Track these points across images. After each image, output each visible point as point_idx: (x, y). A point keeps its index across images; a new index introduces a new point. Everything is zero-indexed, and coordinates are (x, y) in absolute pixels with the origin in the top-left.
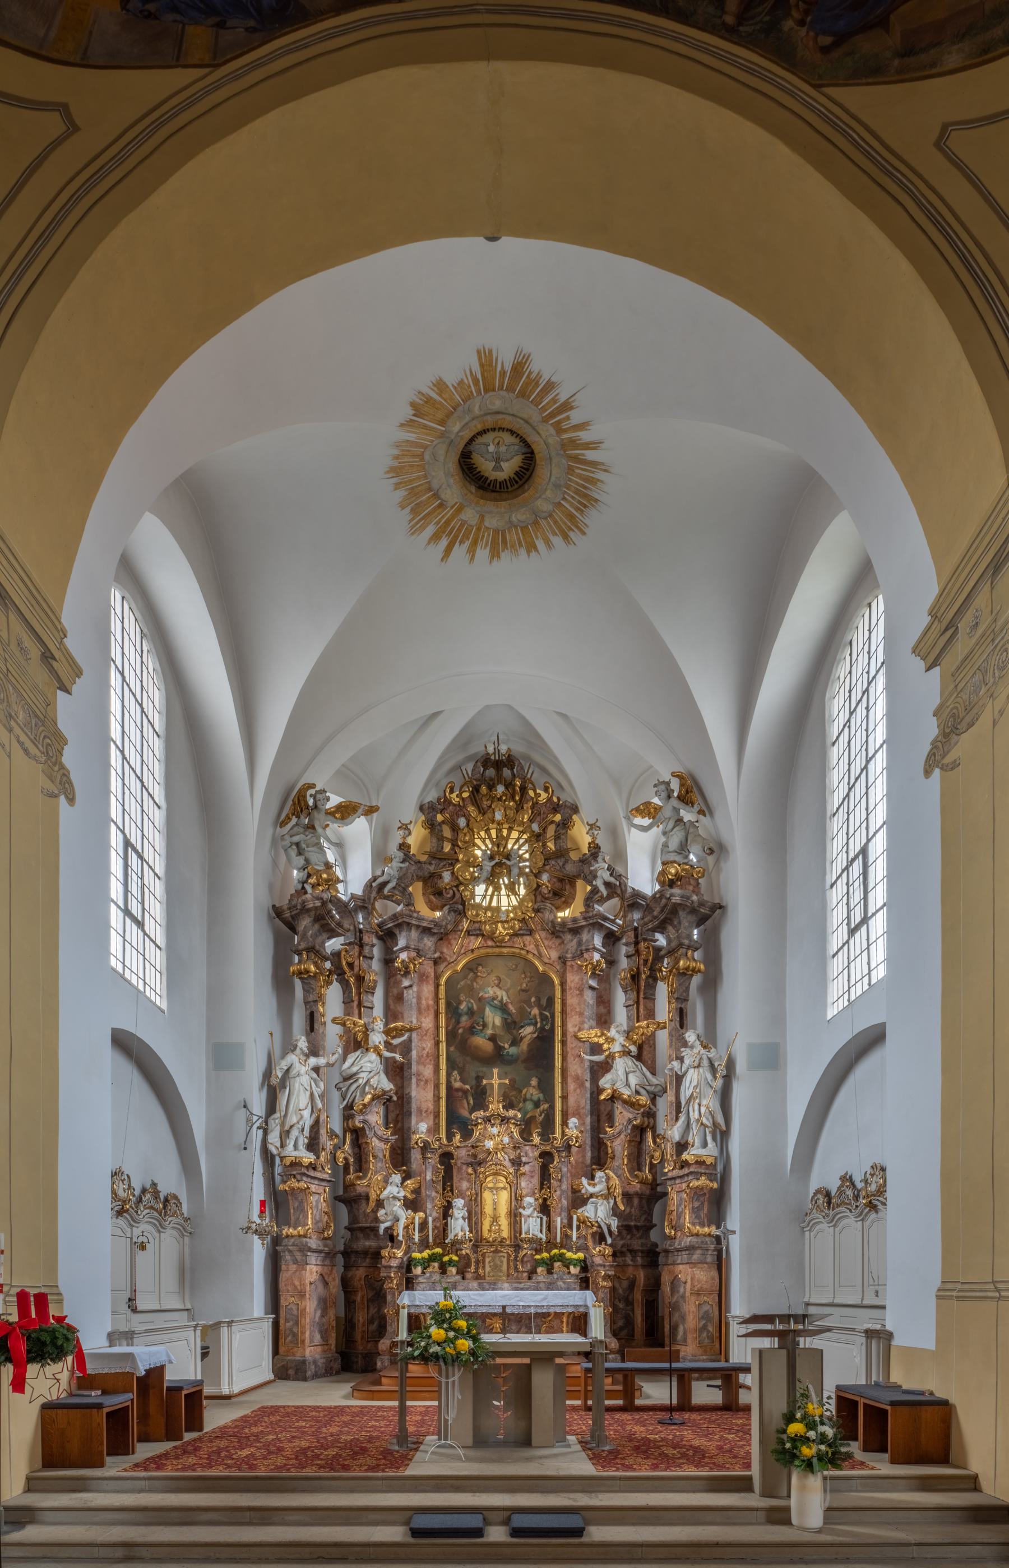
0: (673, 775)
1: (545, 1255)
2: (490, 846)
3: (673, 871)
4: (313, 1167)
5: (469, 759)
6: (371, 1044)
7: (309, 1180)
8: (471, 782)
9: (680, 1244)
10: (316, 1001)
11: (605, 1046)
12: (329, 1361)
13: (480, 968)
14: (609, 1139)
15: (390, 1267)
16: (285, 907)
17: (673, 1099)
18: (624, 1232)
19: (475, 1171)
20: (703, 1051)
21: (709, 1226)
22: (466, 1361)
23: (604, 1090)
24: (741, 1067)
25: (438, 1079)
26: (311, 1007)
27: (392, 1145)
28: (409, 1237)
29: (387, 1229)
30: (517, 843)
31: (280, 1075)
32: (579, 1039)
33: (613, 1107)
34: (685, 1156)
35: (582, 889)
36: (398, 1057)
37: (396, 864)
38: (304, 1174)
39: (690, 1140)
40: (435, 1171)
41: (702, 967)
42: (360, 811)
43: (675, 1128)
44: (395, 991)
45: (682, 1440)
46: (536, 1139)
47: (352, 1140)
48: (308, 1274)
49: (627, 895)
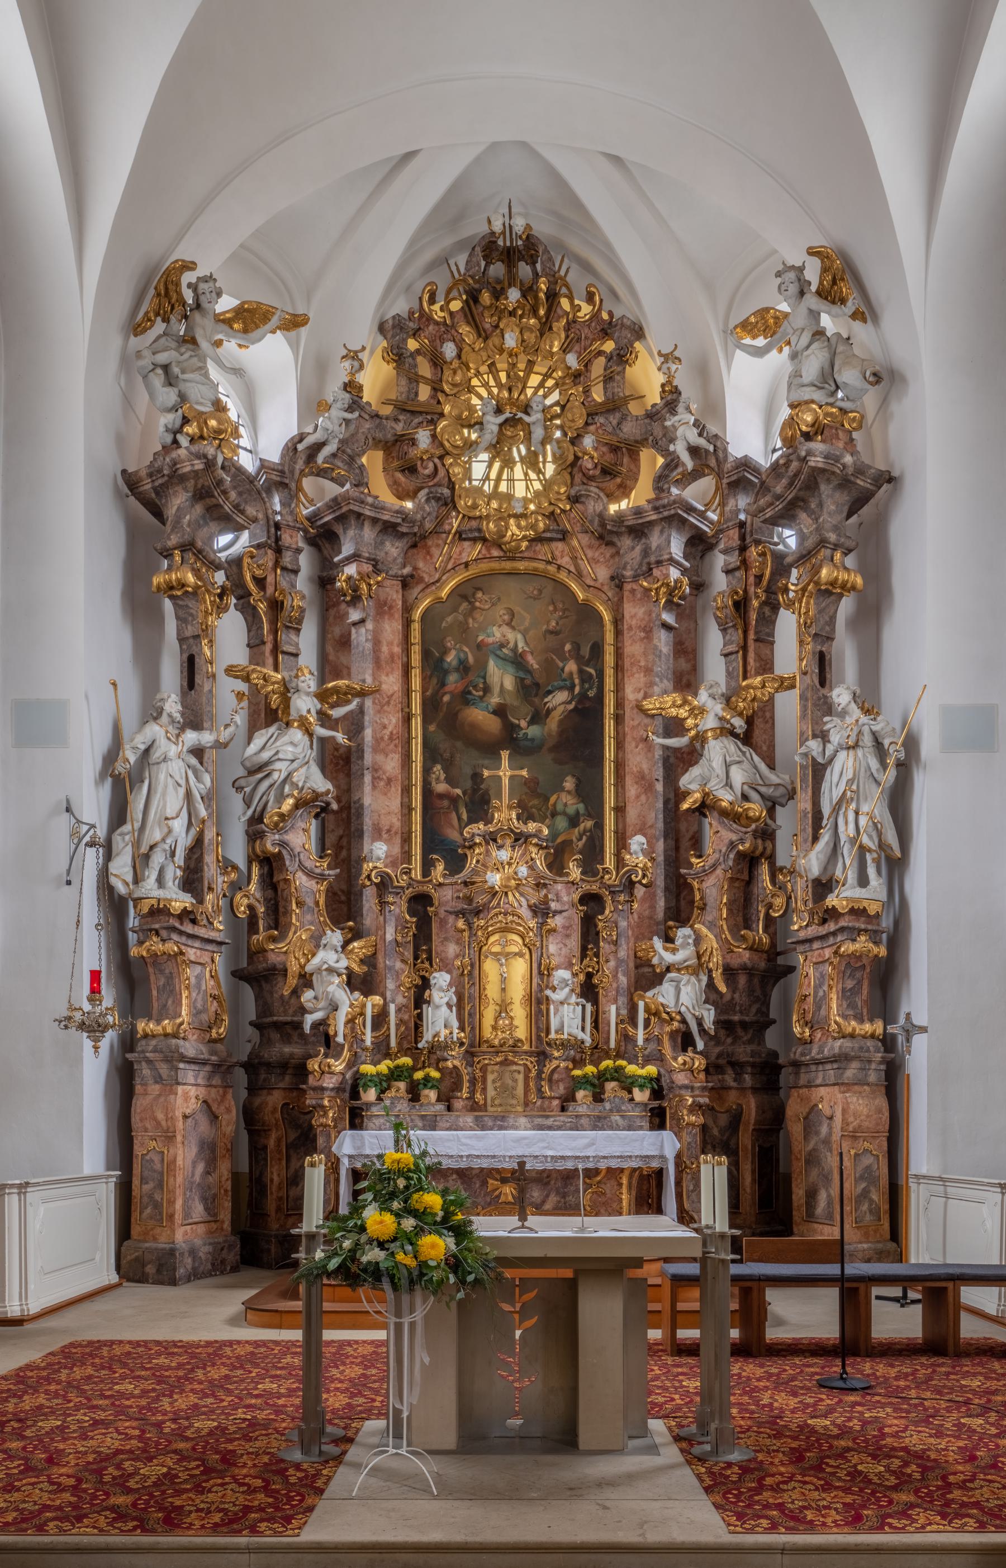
0: (812, 252)
1: (590, 1069)
2: (495, 391)
3: (809, 418)
4: (187, 915)
5: (460, 246)
6: (294, 714)
7: (184, 939)
8: (464, 281)
9: (821, 1051)
10: (197, 637)
11: (690, 722)
12: (219, 1249)
13: (479, 595)
14: (696, 876)
15: (323, 1089)
16: (143, 473)
17: (808, 806)
18: (722, 1033)
19: (470, 925)
20: (864, 719)
21: (871, 1020)
22: (441, 1282)
23: (687, 794)
24: (929, 747)
25: (409, 778)
26: (189, 647)
27: (330, 884)
28: (355, 1038)
29: (316, 1025)
30: (543, 392)
31: (132, 759)
32: (644, 712)
33: (700, 825)
34: (832, 901)
35: (651, 462)
36: (340, 737)
37: (337, 413)
38: (174, 929)
39: (838, 873)
40: (401, 926)
41: (859, 581)
42: (275, 321)
43: (813, 855)
44: (337, 631)
45: (883, 1436)
46: (575, 872)
47: (261, 876)
48: (179, 1101)
49: (728, 466)
